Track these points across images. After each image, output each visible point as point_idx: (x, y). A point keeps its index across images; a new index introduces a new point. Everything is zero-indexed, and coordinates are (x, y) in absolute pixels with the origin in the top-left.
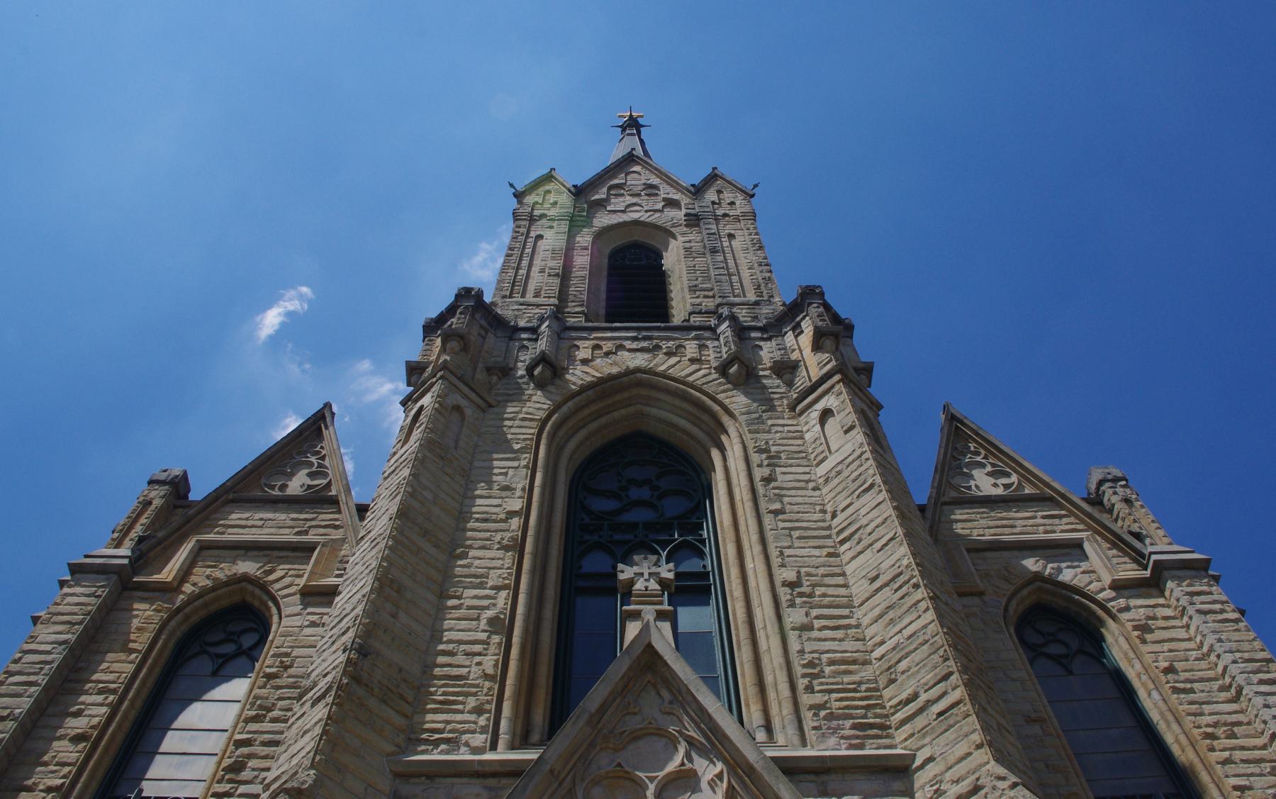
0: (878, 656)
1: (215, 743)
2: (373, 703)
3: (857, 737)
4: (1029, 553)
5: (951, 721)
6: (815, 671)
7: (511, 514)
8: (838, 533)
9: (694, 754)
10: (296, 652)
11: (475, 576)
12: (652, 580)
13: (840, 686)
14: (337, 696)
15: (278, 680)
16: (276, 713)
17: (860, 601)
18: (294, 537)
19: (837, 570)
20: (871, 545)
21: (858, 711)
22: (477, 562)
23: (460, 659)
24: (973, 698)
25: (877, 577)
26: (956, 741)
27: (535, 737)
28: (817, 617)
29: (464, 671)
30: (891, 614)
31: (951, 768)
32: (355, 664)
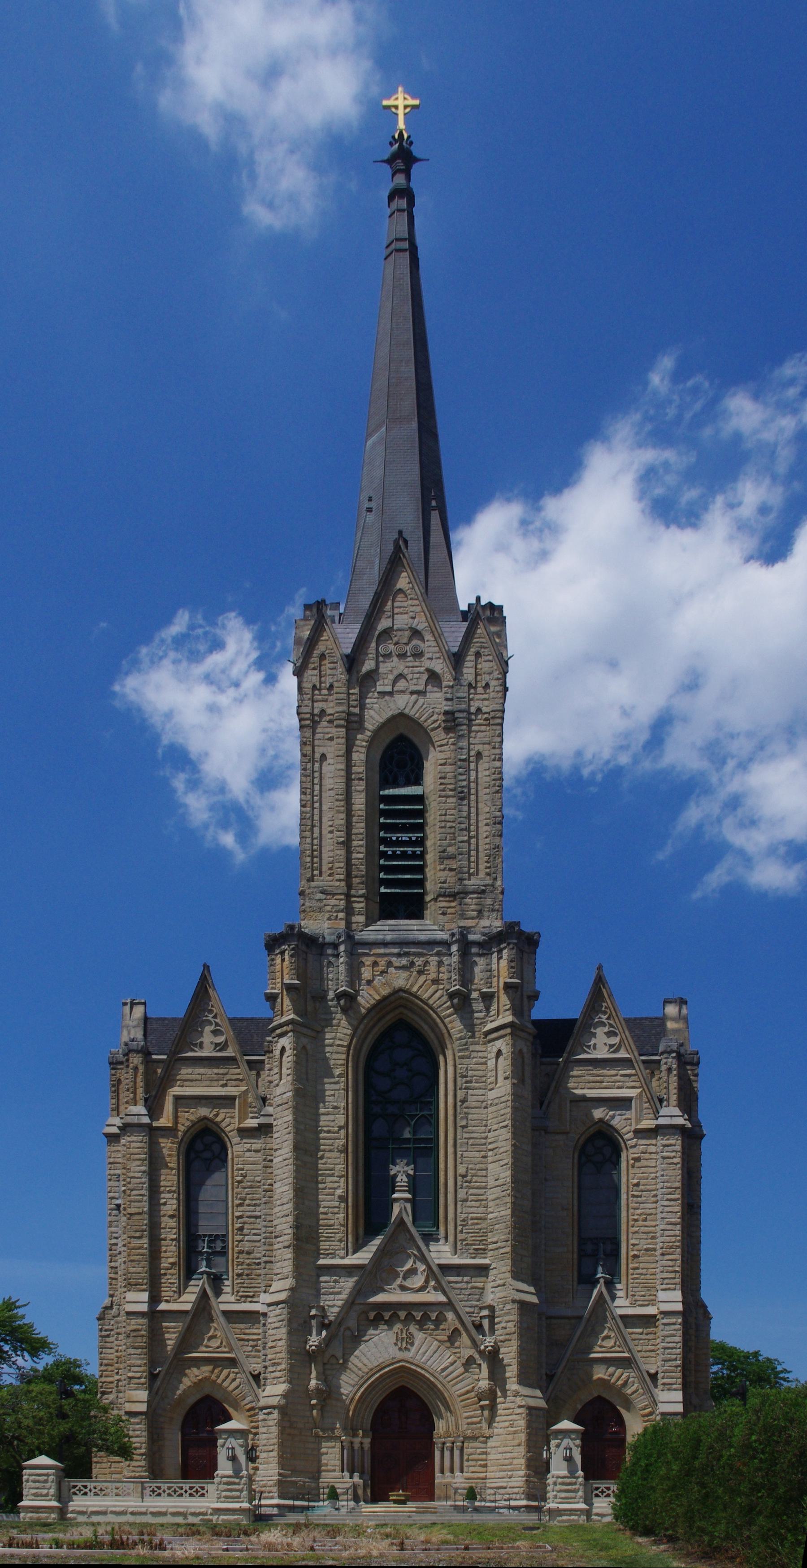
7: (340, 1128)
16: (247, 1202)
19: (483, 1166)
22: (329, 1161)
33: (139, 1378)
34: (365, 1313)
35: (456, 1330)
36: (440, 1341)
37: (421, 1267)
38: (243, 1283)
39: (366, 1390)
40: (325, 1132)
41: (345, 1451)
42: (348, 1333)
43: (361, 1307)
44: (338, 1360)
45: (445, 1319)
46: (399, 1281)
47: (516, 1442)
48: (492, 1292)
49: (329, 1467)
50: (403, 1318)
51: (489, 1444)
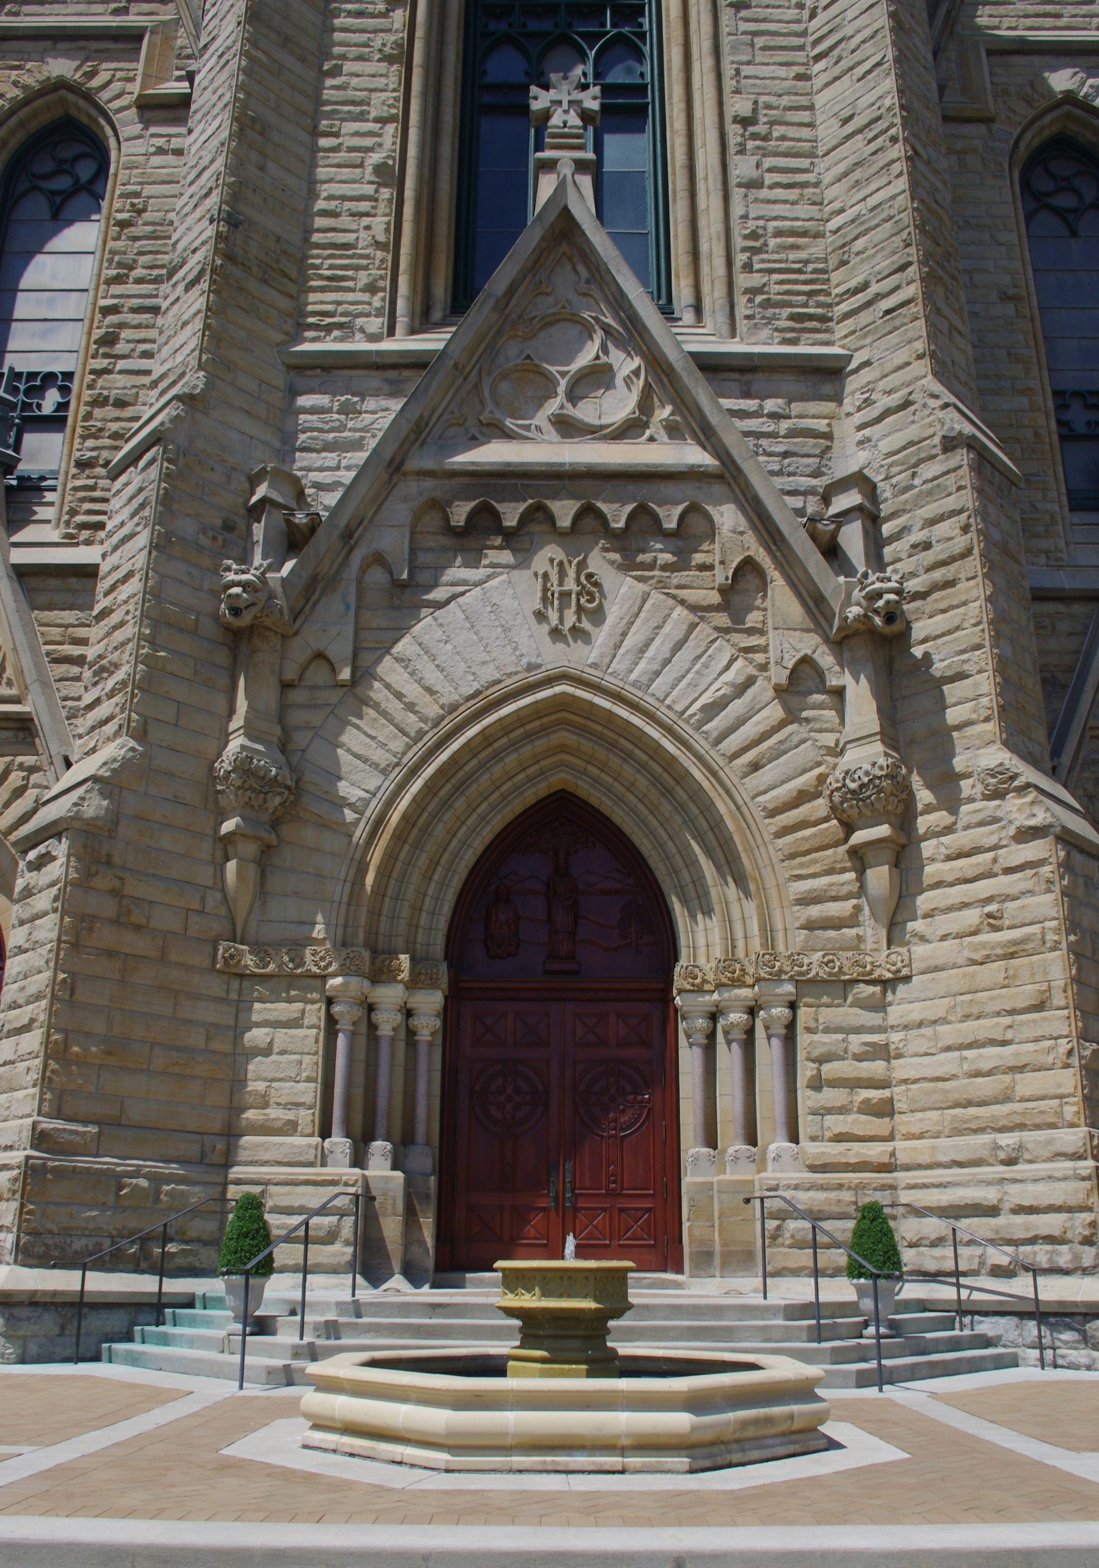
0: (833, 228)
1: (75, 306)
2: (252, 285)
3: (793, 330)
4: (1067, 59)
5: (897, 323)
6: (757, 244)
8: (815, 43)
9: (610, 345)
10: (148, 190)
11: (353, 103)
12: (572, 112)
13: (783, 265)
14: (213, 282)
15: (132, 229)
16: (138, 272)
17: (825, 149)
18: (111, 18)
19: (803, 101)
20: (852, 68)
21: (799, 298)
22: (354, 81)
23: (345, 221)
24: (928, 296)
25: (851, 118)
26: (898, 347)
27: (437, 315)
28: (770, 170)
29: (350, 238)
30: (857, 175)
31: (886, 376)
32: (227, 239)
34: (439, 506)
35: (748, 566)
36: (694, 608)
37: (624, 364)
38: (93, 488)
39: (430, 788)
40: (350, 14)
41: (341, 1041)
42: (377, 576)
43: (428, 483)
44: (333, 670)
45: (711, 532)
46: (552, 406)
47: (1026, 993)
48: (860, 443)
49: (273, 1113)
50: (565, 521)
51: (895, 1014)
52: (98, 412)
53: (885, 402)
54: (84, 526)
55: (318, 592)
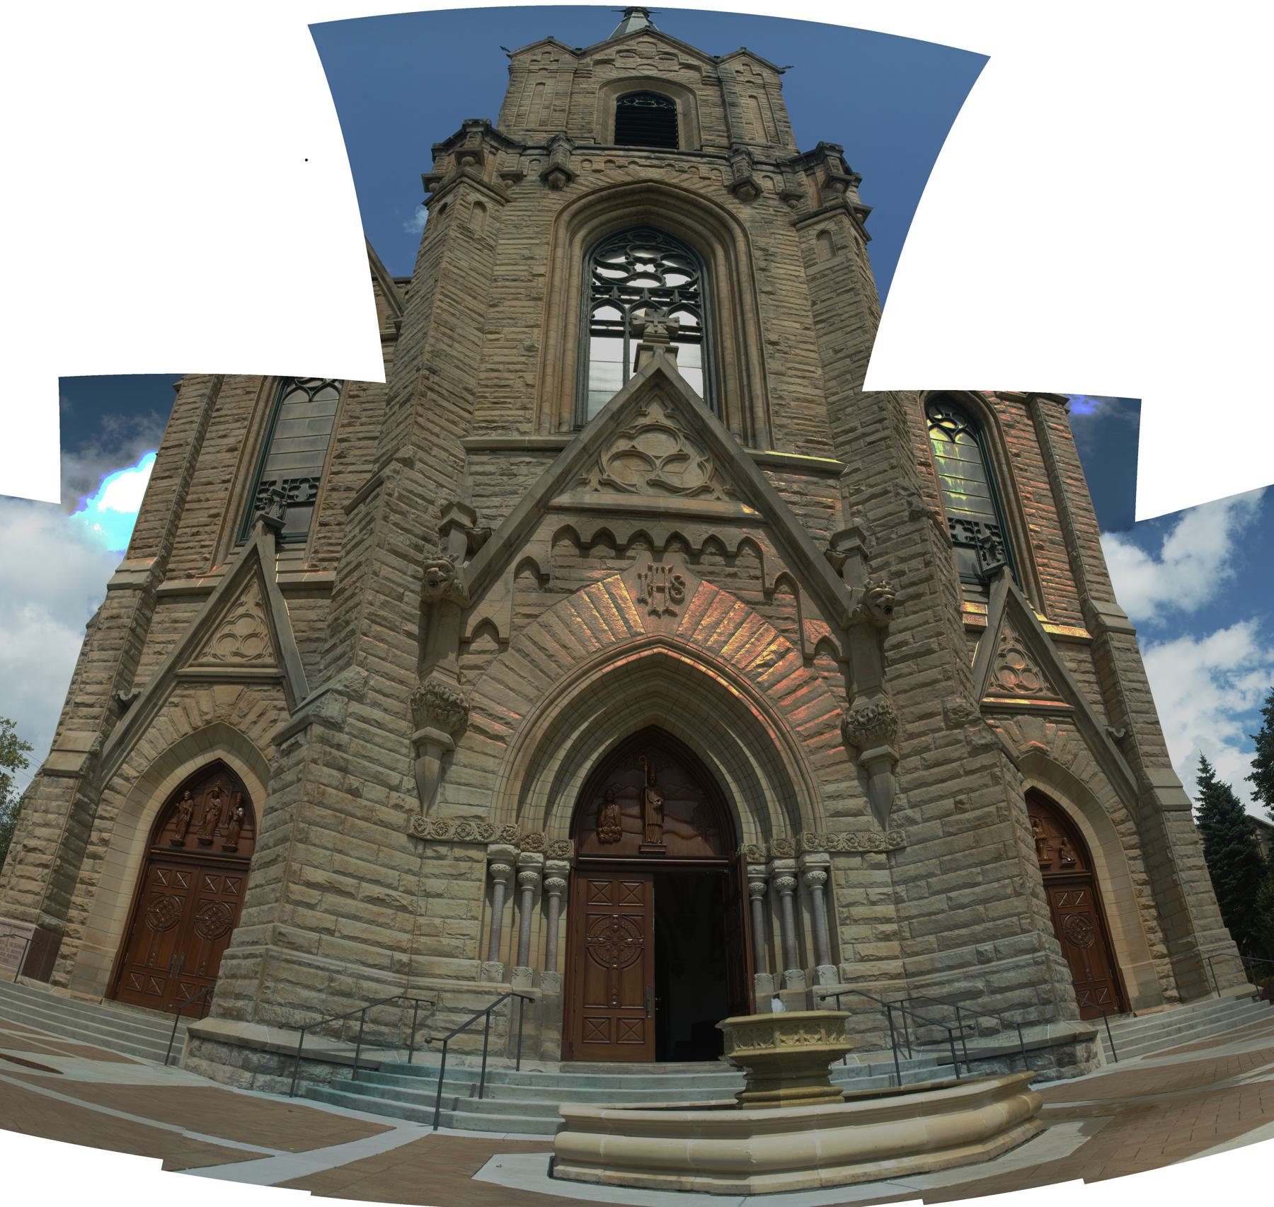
5: (877, 449)
33: (91, 706)
52: (334, 494)
53: (868, 492)
54: (323, 560)
55: (487, 581)
